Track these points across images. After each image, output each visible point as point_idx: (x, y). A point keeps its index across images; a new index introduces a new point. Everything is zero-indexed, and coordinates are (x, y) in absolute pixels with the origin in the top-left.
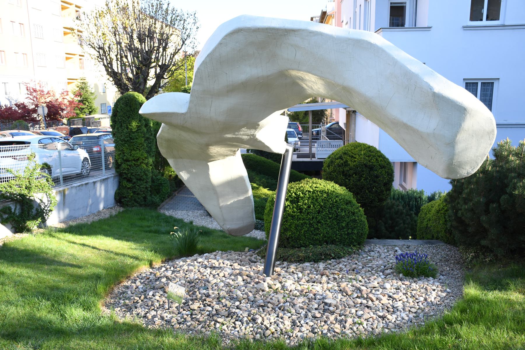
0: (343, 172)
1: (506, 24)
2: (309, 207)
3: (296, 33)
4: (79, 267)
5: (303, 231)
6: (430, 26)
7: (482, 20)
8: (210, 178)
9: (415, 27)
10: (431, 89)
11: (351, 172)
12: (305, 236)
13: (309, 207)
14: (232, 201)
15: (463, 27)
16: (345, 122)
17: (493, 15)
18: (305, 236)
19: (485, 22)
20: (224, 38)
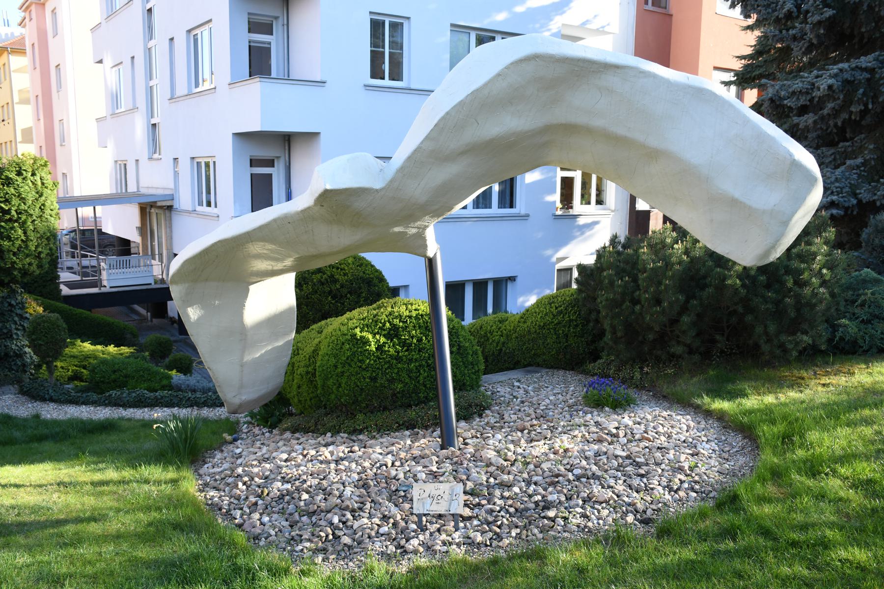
0: (330, 292)
1: (412, 87)
2: (420, 340)
3: (619, 71)
4: (93, 519)
5: (421, 378)
6: (324, 79)
7: (383, 78)
8: (243, 313)
9: (287, 77)
10: (791, 155)
11: (345, 291)
12: (425, 386)
13: (420, 340)
14: (270, 348)
15: (365, 86)
16: (138, 224)
17: (397, 74)
18: (425, 386)
19: (387, 82)
20: (507, 68)
